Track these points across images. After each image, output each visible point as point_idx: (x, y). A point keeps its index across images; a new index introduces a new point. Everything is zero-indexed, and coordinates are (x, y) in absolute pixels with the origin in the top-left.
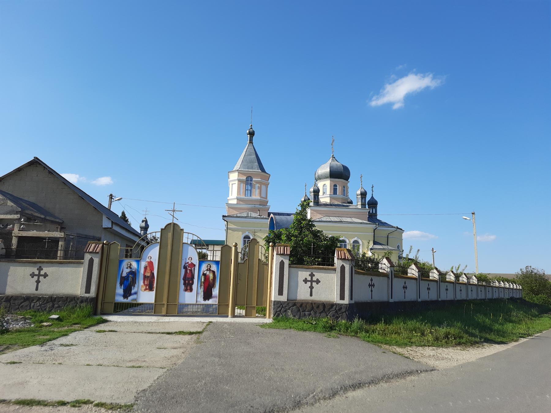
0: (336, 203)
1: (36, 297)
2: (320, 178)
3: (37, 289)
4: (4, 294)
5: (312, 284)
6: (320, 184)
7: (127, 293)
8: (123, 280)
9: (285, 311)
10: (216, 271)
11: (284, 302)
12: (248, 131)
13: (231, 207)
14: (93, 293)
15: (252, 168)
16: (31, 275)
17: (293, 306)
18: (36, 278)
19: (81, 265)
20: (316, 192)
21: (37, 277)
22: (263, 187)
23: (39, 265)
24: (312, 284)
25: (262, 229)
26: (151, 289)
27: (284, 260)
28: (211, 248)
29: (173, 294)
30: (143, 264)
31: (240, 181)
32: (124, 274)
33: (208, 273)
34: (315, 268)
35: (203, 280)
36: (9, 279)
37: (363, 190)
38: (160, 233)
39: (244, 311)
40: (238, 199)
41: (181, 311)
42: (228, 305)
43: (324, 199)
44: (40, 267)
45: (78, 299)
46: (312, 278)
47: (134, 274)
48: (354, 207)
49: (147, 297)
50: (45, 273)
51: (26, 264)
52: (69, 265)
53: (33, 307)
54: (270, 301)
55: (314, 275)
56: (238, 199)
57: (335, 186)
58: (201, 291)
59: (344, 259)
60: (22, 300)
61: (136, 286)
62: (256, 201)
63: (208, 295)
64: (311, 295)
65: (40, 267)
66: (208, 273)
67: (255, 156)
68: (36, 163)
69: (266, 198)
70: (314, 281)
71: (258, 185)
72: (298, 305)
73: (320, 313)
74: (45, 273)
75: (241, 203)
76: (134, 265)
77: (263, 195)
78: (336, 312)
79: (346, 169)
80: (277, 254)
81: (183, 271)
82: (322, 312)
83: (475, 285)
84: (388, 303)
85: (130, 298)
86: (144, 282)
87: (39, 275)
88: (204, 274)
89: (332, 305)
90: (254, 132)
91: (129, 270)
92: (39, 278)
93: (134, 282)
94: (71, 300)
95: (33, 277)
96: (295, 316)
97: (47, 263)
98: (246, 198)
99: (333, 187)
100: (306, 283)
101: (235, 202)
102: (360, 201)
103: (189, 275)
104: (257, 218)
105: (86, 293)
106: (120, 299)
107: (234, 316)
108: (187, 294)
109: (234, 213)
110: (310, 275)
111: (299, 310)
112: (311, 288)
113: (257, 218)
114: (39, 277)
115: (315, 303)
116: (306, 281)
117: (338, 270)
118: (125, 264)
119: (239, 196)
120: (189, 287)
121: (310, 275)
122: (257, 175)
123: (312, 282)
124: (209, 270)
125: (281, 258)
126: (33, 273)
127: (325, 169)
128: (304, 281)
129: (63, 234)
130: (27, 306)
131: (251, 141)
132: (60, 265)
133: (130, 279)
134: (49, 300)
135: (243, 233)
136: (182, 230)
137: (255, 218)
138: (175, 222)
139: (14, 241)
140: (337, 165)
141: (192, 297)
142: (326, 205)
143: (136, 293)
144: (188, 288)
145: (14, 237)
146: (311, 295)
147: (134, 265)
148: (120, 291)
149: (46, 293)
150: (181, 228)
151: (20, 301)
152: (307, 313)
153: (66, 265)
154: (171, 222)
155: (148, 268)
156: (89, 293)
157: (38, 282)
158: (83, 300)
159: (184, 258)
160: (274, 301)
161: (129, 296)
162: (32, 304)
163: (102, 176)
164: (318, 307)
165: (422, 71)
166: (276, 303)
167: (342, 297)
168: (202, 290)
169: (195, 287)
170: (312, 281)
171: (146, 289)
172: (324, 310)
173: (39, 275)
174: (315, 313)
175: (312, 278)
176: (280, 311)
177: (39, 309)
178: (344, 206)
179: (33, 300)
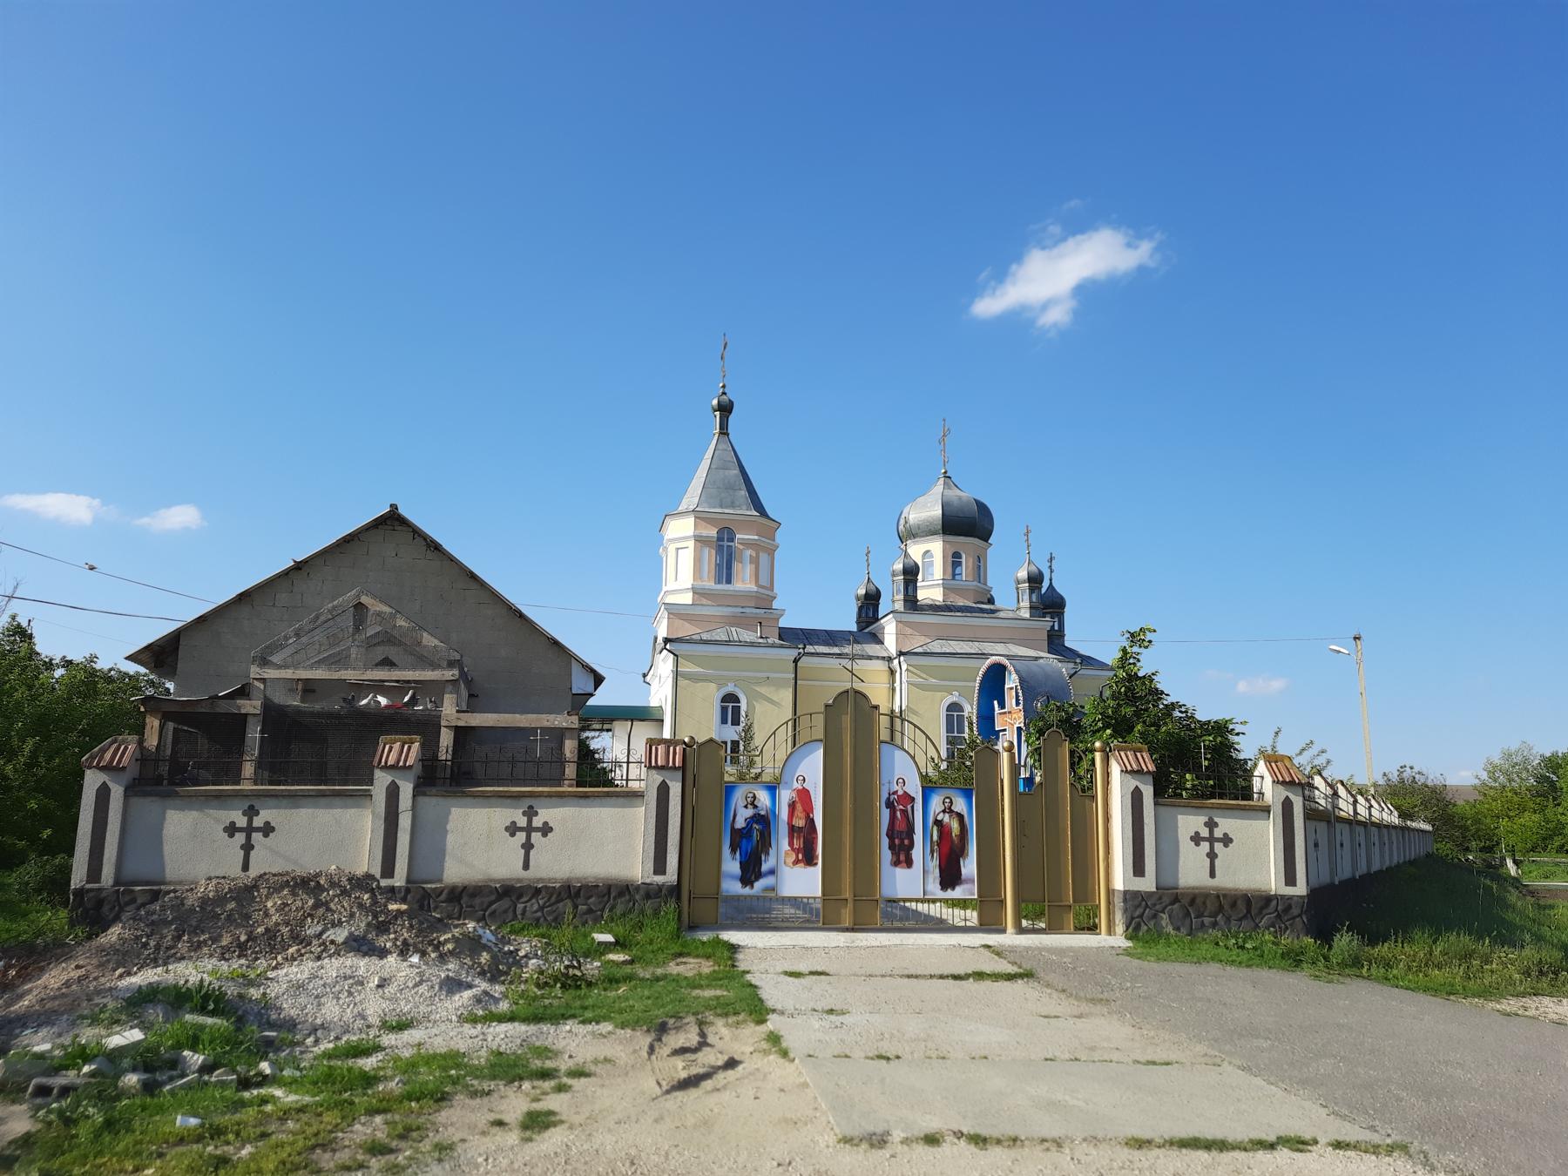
0: (961, 602)
1: (529, 886)
2: (910, 534)
3: (526, 866)
4: (440, 881)
5: (1212, 848)
6: (916, 551)
7: (751, 872)
8: (739, 838)
9: (1155, 916)
10: (965, 813)
11: (1150, 894)
12: (715, 402)
13: (675, 612)
14: (671, 876)
15: (732, 506)
16: (507, 829)
17: (1172, 903)
18: (521, 837)
19: (638, 801)
20: (911, 574)
21: (254, 835)
22: (764, 557)
23: (528, 802)
24: (1212, 848)
25: (771, 675)
26: (809, 860)
27: (1142, 787)
28: (621, 728)
29: (866, 876)
30: (785, 796)
31: (700, 540)
32: (740, 823)
33: (946, 818)
34: (1219, 807)
35: (935, 838)
36: (450, 838)
37: (1033, 568)
38: (822, 717)
39: (975, 914)
40: (696, 591)
41: (901, 918)
42: (1003, 902)
43: (930, 592)
44: (531, 807)
45: (638, 888)
46: (1211, 832)
47: (763, 822)
48: (1011, 615)
49: (803, 882)
50: (546, 823)
51: (493, 800)
52: (604, 800)
53: (524, 913)
54: (1110, 892)
55: (1216, 825)
56: (695, 591)
57: (957, 555)
58: (934, 866)
59: (1137, 773)
60: (493, 897)
61: (772, 852)
62: (746, 595)
63: (950, 877)
64: (1212, 874)
65: (531, 807)
66: (946, 818)
67: (737, 471)
68: (393, 520)
69: (771, 588)
70: (1218, 840)
71: (748, 553)
72: (1185, 901)
73: (1240, 920)
74: (546, 823)
75: (705, 601)
76: (763, 798)
77: (764, 581)
78: (1279, 916)
79: (983, 509)
80: (1125, 771)
81: (886, 813)
82: (1245, 917)
83: (1395, 827)
84: (1331, 886)
85: (760, 885)
86: (791, 844)
87: (529, 829)
88: (938, 823)
89: (1267, 899)
90: (731, 404)
91: (750, 812)
92: (528, 837)
93: (765, 843)
94: (621, 894)
95: (231, 836)
96: (1178, 929)
97: (550, 795)
98: (719, 587)
99: (950, 559)
100: (1197, 844)
101: (687, 599)
102: (1026, 597)
103: (901, 826)
104: (758, 645)
105: (656, 872)
106: (733, 887)
107: (1021, 931)
108: (900, 872)
109: (686, 630)
110: (1206, 824)
111: (1188, 914)
112: (1212, 856)
113: (758, 645)
114: (529, 833)
115: (1225, 896)
116: (1197, 839)
117: (1277, 811)
118: (739, 798)
119: (699, 584)
120: (902, 856)
121: (1206, 824)
122: (747, 525)
123: (1213, 841)
124: (948, 810)
125: (1133, 783)
126: (514, 823)
127: (929, 509)
128: (1192, 839)
129: (575, 719)
130: (505, 911)
131: (724, 431)
132: (582, 801)
133: (756, 835)
134: (564, 895)
135: (720, 686)
136: (876, 707)
137: (752, 645)
138: (858, 686)
139: (446, 739)
140: (960, 498)
141: (910, 882)
142: (934, 608)
143: (772, 872)
144: (902, 857)
145: (443, 730)
146: (1212, 874)
147: (763, 798)
148: (732, 865)
149: (551, 875)
150: (874, 703)
151: (487, 900)
152: (1207, 920)
153: (598, 801)
154: (848, 686)
155: (799, 807)
156: (664, 873)
157: (528, 846)
158: (652, 893)
159: (885, 780)
160: (1125, 892)
161: (757, 879)
162: (520, 906)
163: (169, 506)
164: (1234, 905)
165: (1133, 223)
166: (1129, 896)
167: (1290, 880)
168: (936, 862)
169: (917, 853)
170: (1211, 840)
171: (796, 862)
172: (1249, 911)
173: (529, 829)
174: (1228, 920)
175: (1211, 832)
176: (1141, 916)
177: (538, 920)
178: (982, 611)
179: (520, 896)
